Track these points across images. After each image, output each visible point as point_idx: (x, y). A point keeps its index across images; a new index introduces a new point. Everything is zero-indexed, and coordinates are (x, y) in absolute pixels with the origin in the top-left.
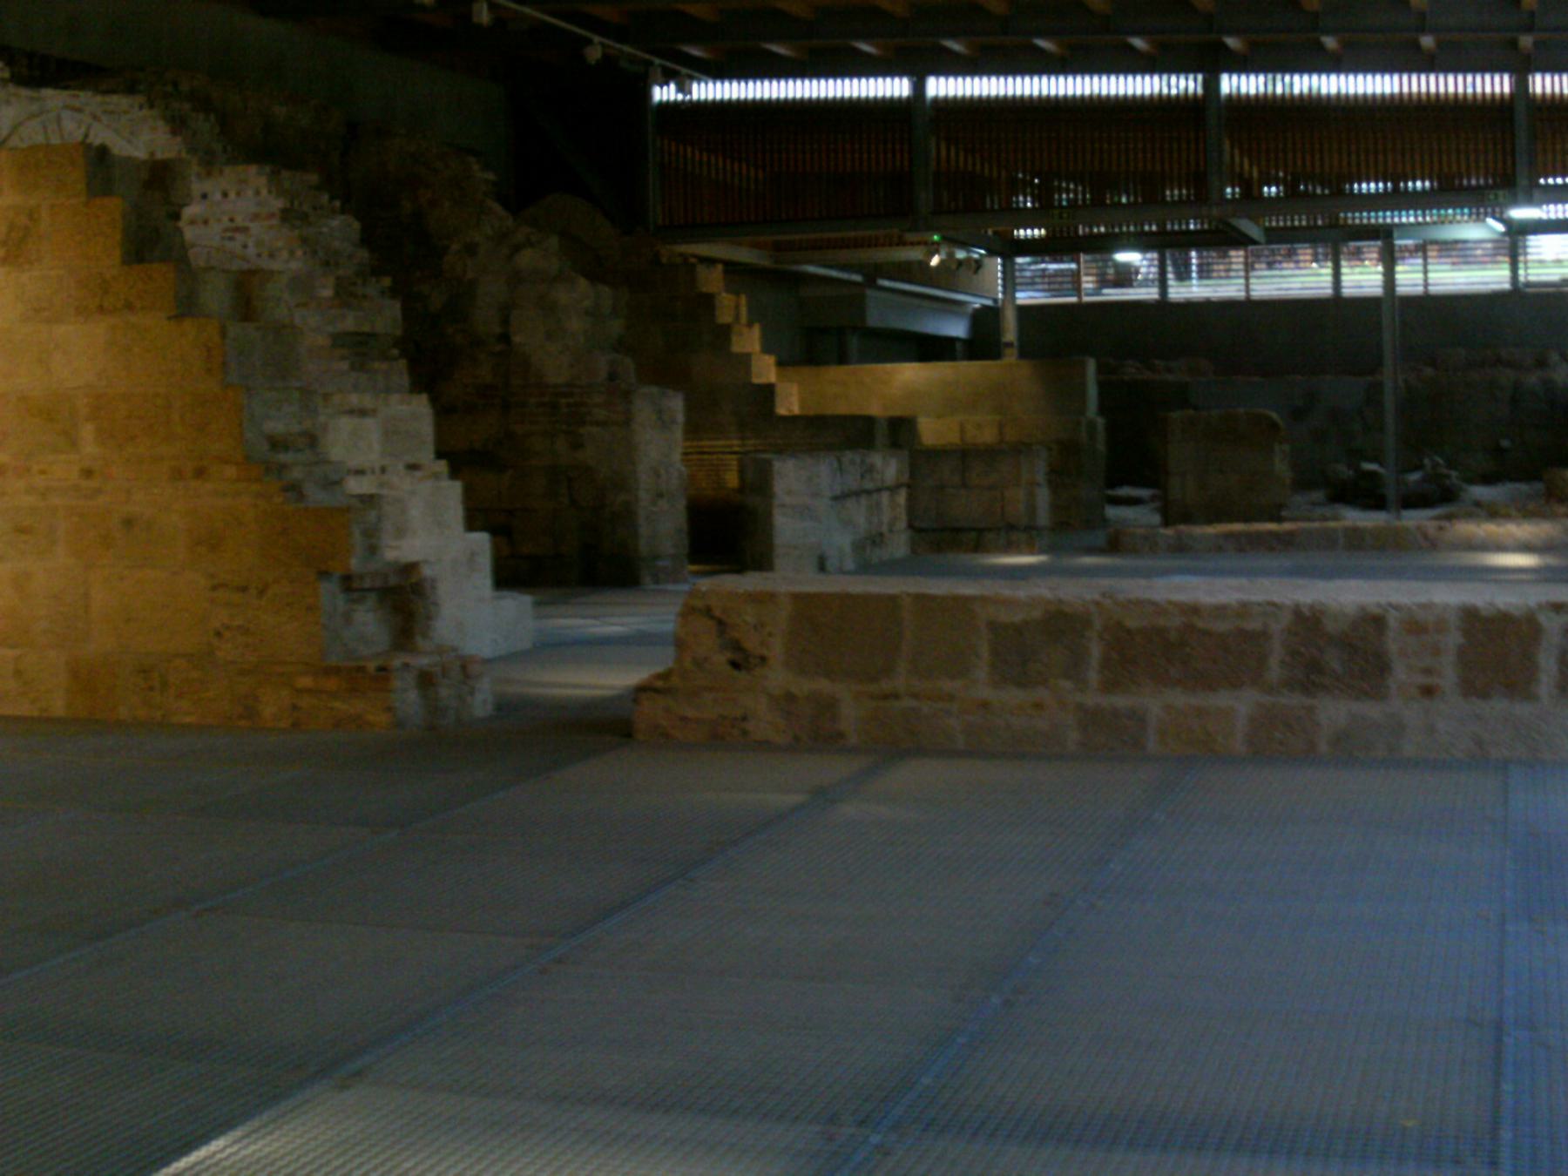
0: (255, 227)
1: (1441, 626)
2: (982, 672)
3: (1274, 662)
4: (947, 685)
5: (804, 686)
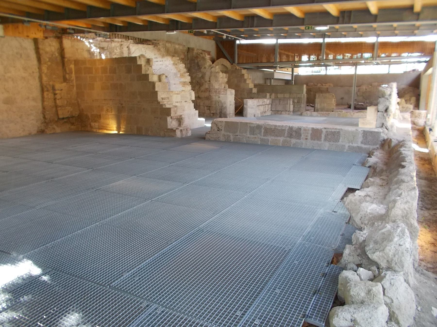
0: (169, 66)
1: (308, 130)
2: (248, 133)
3: (286, 134)
4: (244, 134)
5: (226, 134)
